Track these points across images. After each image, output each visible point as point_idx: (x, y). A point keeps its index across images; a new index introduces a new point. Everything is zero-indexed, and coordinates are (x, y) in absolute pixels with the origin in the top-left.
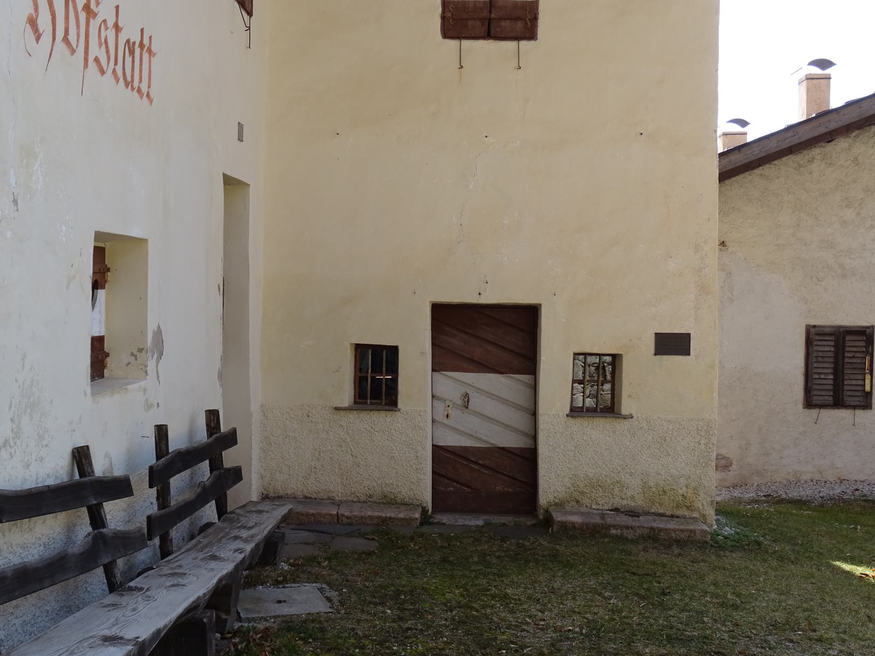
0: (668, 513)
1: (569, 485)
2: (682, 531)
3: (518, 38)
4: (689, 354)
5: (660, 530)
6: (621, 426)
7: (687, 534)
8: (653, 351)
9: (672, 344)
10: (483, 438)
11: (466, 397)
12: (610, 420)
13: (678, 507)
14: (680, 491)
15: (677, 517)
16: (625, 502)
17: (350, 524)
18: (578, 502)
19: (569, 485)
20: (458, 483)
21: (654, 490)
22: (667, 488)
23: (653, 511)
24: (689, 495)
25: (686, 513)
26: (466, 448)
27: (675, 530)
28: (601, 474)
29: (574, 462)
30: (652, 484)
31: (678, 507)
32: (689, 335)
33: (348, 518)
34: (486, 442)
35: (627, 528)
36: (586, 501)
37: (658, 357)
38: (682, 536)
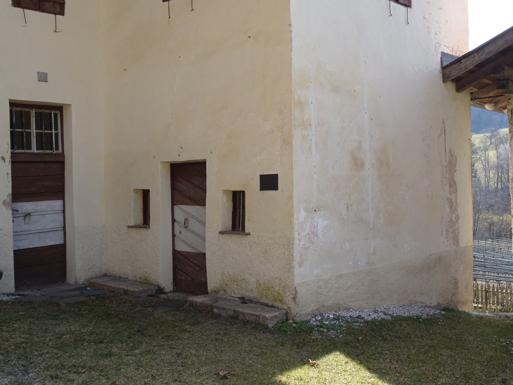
0: (270, 304)
1: (221, 279)
2: (252, 315)
3: (55, 14)
4: (277, 189)
5: (241, 313)
6: (246, 240)
7: (254, 318)
8: (259, 189)
9: (269, 182)
10: (195, 247)
11: (186, 220)
12: (239, 236)
13: (275, 300)
14: (276, 289)
15: (274, 307)
16: (247, 294)
17: (113, 292)
18: (225, 291)
19: (221, 279)
20: (186, 274)
21: (263, 286)
22: (270, 286)
23: (262, 301)
24: (281, 292)
25: (280, 305)
26: (188, 253)
27: (248, 314)
28: (235, 273)
29: (227, 264)
30: (262, 282)
31: (275, 300)
32: (276, 175)
33: (113, 288)
34: (193, 248)
35: (223, 309)
36: (229, 291)
37: (262, 191)
38: (252, 319)
